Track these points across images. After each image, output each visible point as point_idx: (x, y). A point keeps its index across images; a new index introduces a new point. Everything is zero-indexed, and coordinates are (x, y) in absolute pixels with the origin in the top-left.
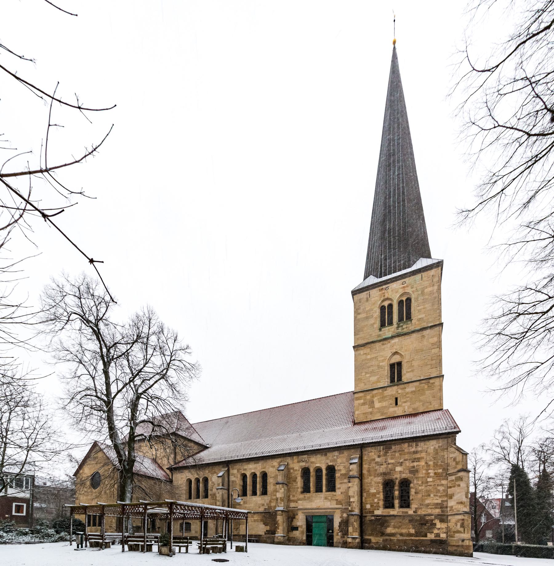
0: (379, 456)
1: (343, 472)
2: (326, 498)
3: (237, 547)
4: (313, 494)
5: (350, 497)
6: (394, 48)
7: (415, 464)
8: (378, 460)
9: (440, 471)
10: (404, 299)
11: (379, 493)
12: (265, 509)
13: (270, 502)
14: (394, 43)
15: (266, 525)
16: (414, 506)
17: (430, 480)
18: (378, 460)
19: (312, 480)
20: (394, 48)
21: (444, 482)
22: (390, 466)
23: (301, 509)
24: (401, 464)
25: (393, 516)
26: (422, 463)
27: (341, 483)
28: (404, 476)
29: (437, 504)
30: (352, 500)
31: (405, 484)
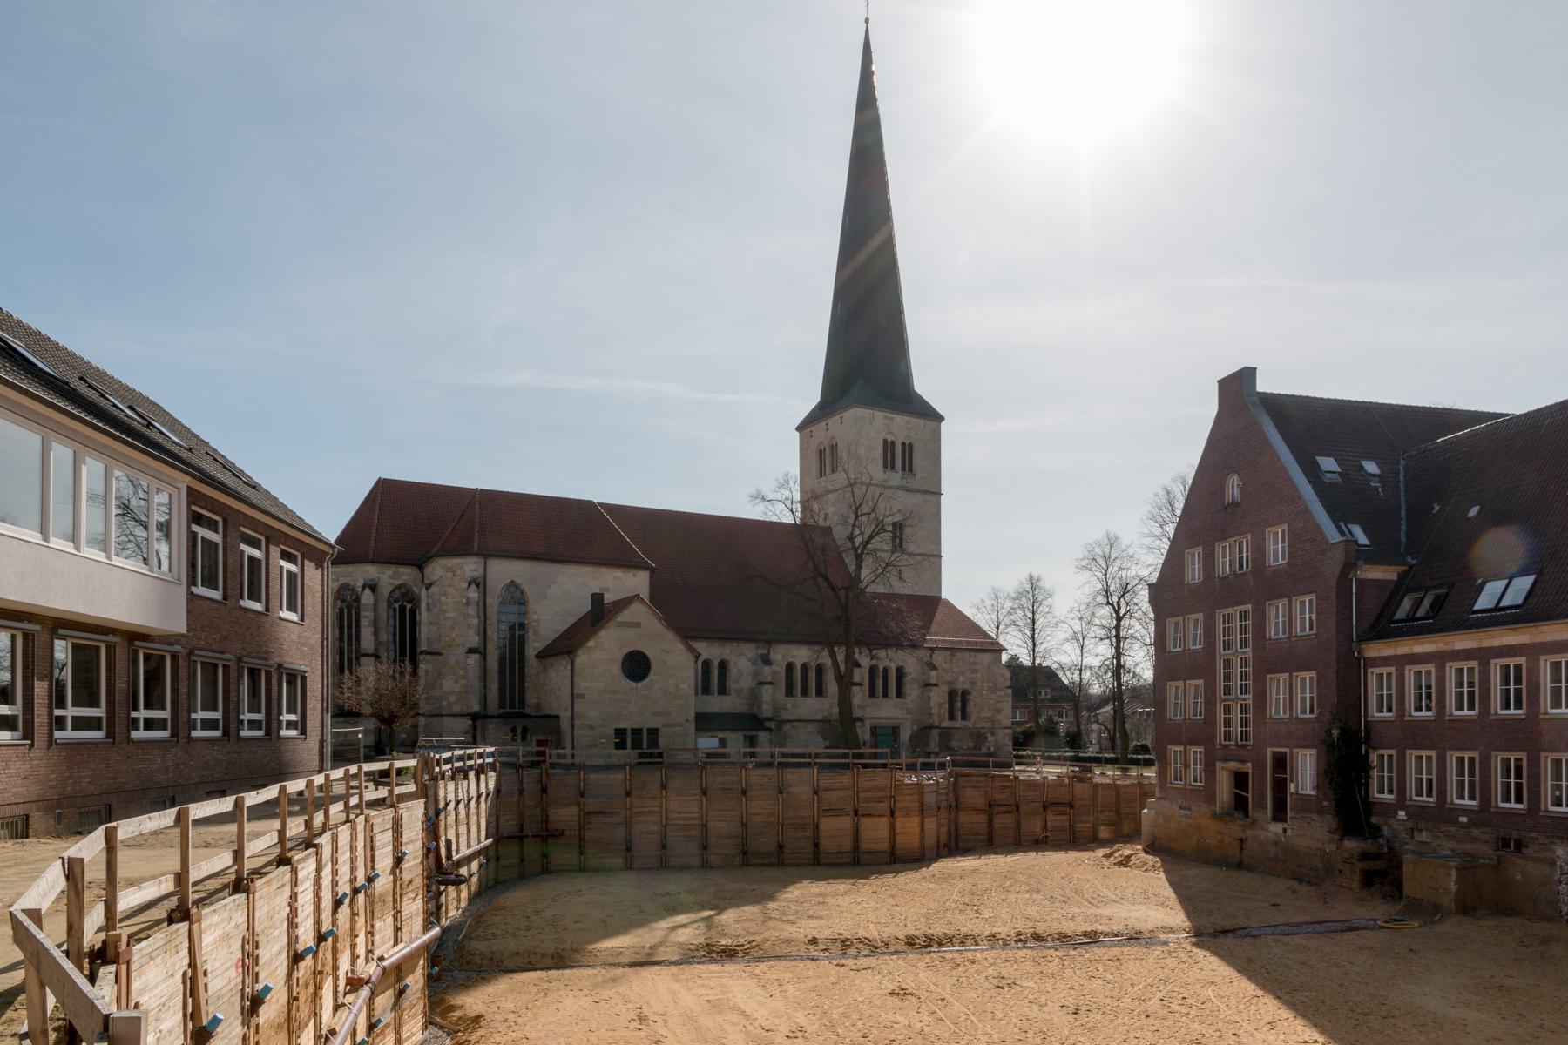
0: (946, 663)
1: (913, 675)
2: (896, 706)
3: (1473, 668)
4: (880, 700)
5: (931, 708)
6: (867, 27)
7: (974, 675)
8: (944, 666)
9: (991, 685)
10: (907, 443)
11: (944, 703)
12: (825, 717)
13: (831, 707)
14: (867, 21)
15: (825, 739)
16: (973, 719)
17: (984, 693)
18: (944, 666)
19: (880, 682)
20: (867, 27)
21: (994, 696)
22: (955, 674)
23: (868, 718)
24: (963, 673)
25: (956, 728)
26: (979, 675)
27: (911, 689)
28: (966, 687)
29: (989, 718)
30: (933, 711)
31: (965, 694)
